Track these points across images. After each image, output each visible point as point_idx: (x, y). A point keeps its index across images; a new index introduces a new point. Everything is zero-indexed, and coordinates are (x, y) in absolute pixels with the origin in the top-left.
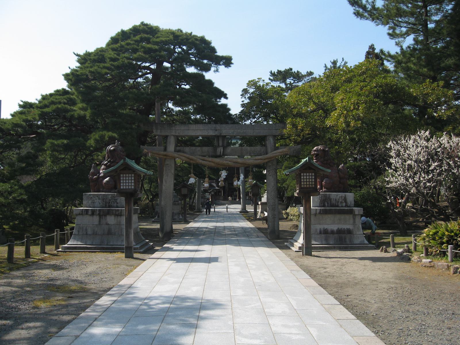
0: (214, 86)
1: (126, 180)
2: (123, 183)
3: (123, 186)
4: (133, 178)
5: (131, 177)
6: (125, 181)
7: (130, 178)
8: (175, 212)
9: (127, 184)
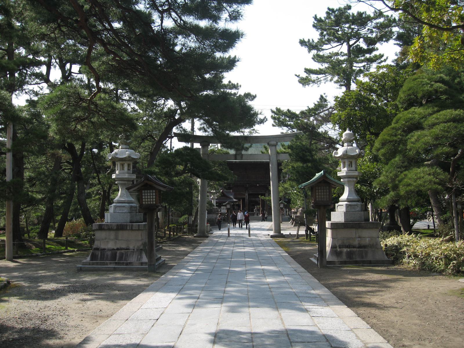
0: (223, 83)
1: (150, 196)
2: (145, 199)
3: (145, 201)
4: (154, 194)
5: (153, 193)
6: (146, 197)
7: (151, 194)
8: (131, 247)
9: (149, 200)
